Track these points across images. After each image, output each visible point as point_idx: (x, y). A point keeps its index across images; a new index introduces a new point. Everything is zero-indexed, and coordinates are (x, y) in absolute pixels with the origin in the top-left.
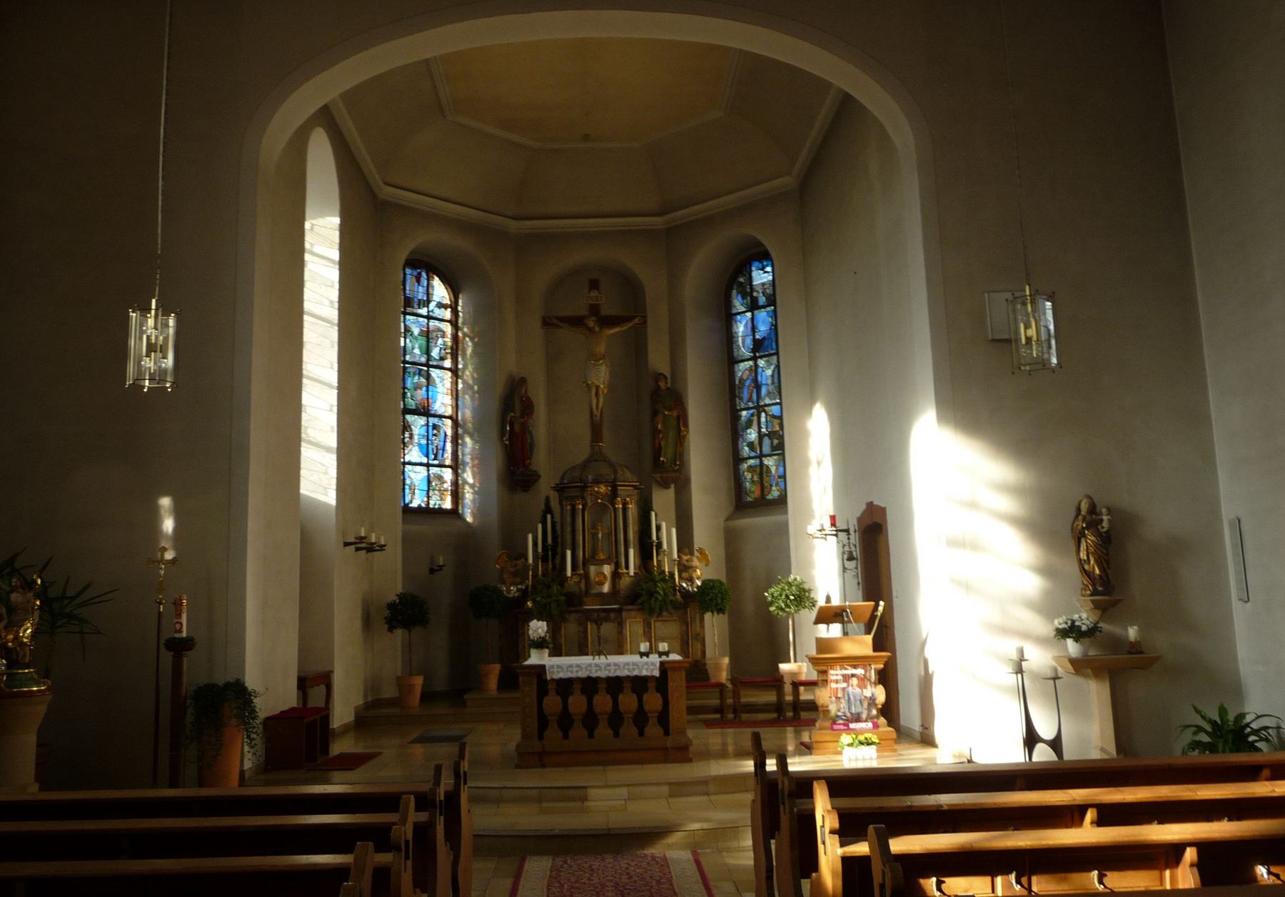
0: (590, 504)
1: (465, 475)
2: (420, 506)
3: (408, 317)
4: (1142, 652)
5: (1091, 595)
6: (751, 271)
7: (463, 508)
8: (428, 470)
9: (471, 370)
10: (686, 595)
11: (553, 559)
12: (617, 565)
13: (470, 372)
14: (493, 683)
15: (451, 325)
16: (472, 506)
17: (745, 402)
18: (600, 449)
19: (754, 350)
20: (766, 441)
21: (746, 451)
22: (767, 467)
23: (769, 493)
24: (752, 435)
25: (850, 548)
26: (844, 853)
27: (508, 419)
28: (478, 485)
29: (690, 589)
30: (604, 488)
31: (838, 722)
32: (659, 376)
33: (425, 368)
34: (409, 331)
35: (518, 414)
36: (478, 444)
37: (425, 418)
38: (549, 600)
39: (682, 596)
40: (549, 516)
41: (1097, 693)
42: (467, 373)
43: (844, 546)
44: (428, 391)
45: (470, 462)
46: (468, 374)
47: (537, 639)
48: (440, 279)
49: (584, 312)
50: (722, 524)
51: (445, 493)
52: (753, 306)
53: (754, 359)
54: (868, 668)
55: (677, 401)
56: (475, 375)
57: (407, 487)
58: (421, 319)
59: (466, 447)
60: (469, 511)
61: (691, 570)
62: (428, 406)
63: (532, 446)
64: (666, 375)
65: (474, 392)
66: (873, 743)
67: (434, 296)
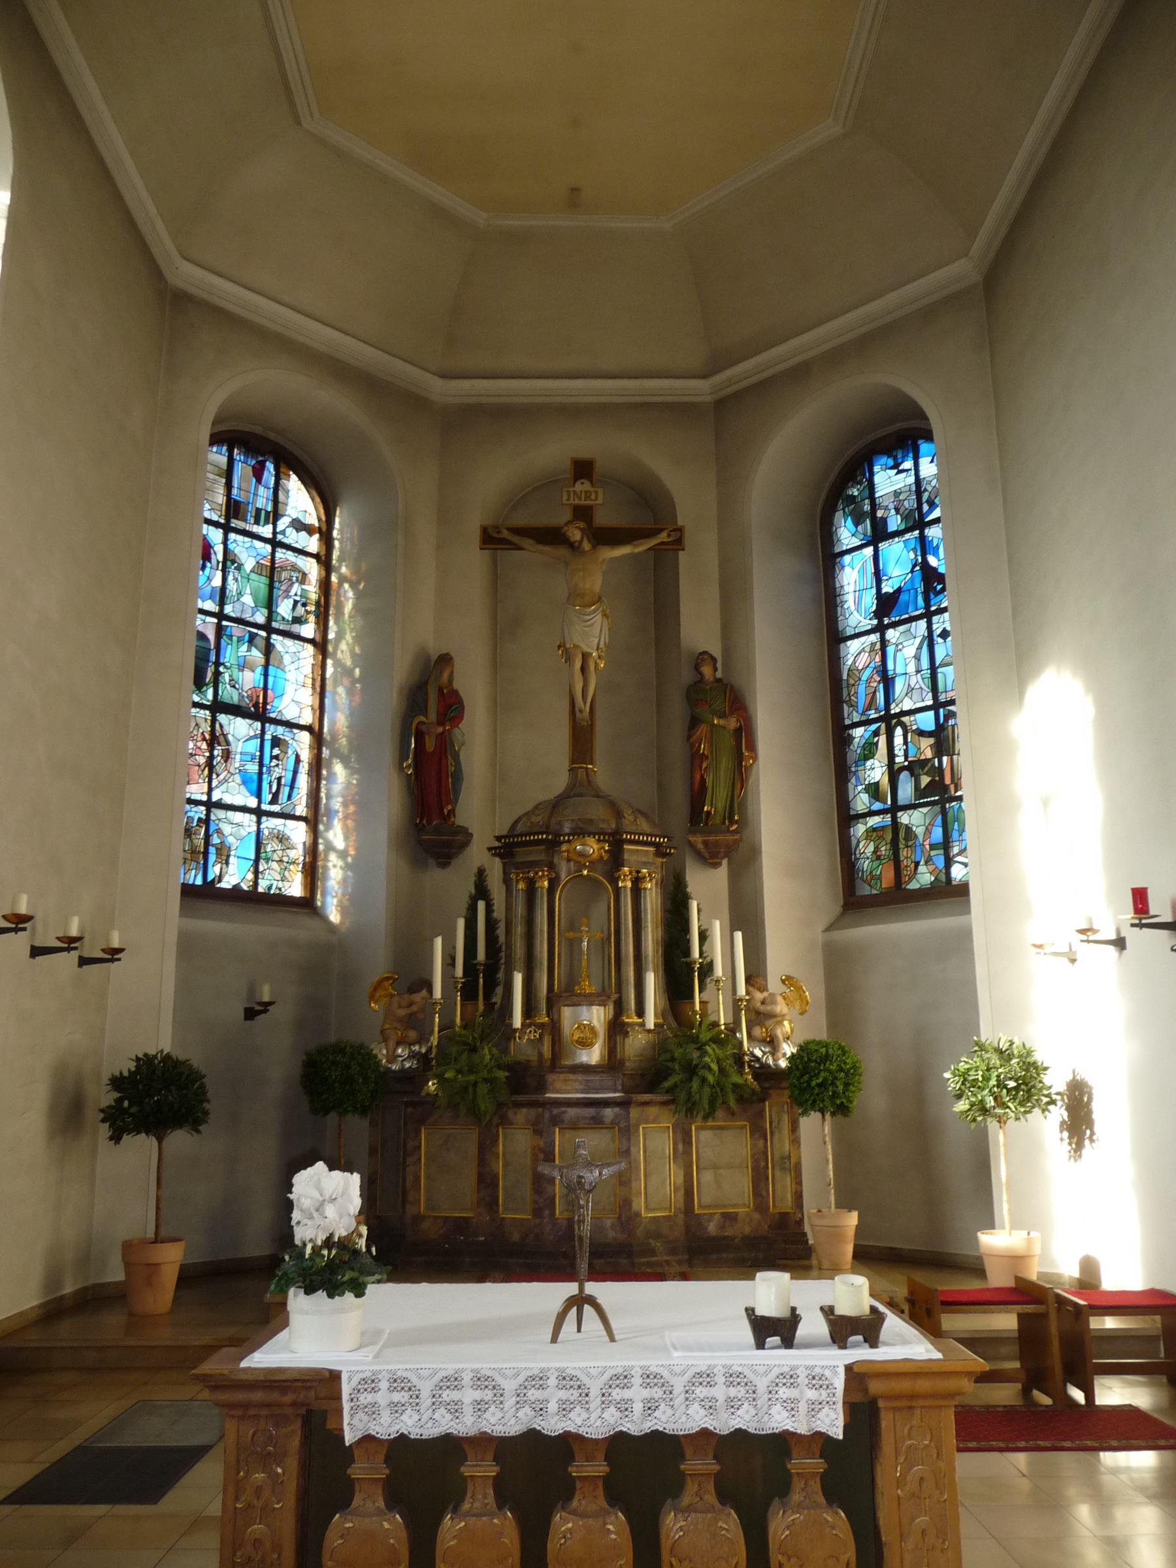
0: (564, 877)
1: (330, 835)
2: (236, 888)
3: (232, 536)
6: (872, 474)
7: (324, 895)
8: (259, 823)
9: (350, 641)
10: (765, 1074)
11: (488, 994)
15: (319, 561)
16: (340, 892)
17: (860, 712)
18: (587, 775)
20: (904, 778)
21: (862, 802)
22: (908, 829)
23: (911, 878)
24: (876, 771)
27: (414, 726)
29: (771, 1062)
30: (596, 846)
32: (704, 657)
33: (263, 634)
34: (233, 562)
35: (433, 716)
36: (355, 776)
37: (258, 725)
38: (472, 1078)
39: (756, 1077)
40: (481, 905)
42: (343, 646)
44: (266, 675)
45: (341, 810)
46: (344, 649)
47: (316, 1251)
48: (300, 479)
49: (562, 517)
50: (820, 938)
51: (292, 867)
53: (881, 629)
56: (357, 650)
57: (212, 850)
58: (258, 544)
59: (335, 782)
60: (335, 901)
61: (770, 1023)
62: (265, 703)
63: (458, 777)
64: (715, 655)
65: (354, 681)
67: (288, 508)
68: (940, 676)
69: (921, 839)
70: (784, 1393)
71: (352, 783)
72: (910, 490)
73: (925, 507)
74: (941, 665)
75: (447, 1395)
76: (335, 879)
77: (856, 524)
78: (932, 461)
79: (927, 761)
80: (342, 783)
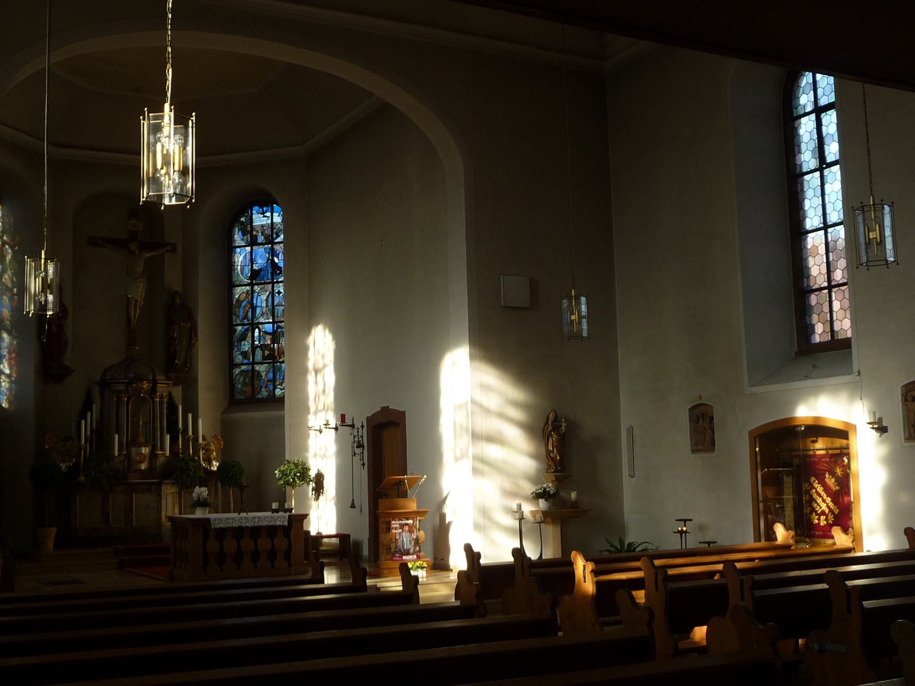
4: (577, 507)
5: (554, 472)
6: (252, 214)
9: (10, 274)
12: (154, 448)
13: (9, 276)
14: (51, 545)
16: (8, 394)
17: (240, 319)
19: (251, 278)
21: (239, 359)
22: (259, 372)
23: (259, 393)
24: (246, 346)
25: (359, 439)
26: (597, 580)
28: (15, 376)
30: (147, 385)
31: (396, 555)
36: (15, 340)
39: (205, 473)
41: (552, 532)
43: (354, 437)
45: (7, 355)
52: (253, 243)
53: (251, 285)
54: (415, 519)
55: (191, 317)
56: (15, 279)
65: (13, 295)
66: (424, 567)
68: (276, 310)
69: (264, 377)
70: (279, 519)
71: (13, 343)
72: (268, 226)
73: (275, 236)
74: (277, 306)
75: (227, 521)
76: (4, 387)
77: (244, 235)
78: (279, 216)
79: (268, 345)
80: (7, 343)
